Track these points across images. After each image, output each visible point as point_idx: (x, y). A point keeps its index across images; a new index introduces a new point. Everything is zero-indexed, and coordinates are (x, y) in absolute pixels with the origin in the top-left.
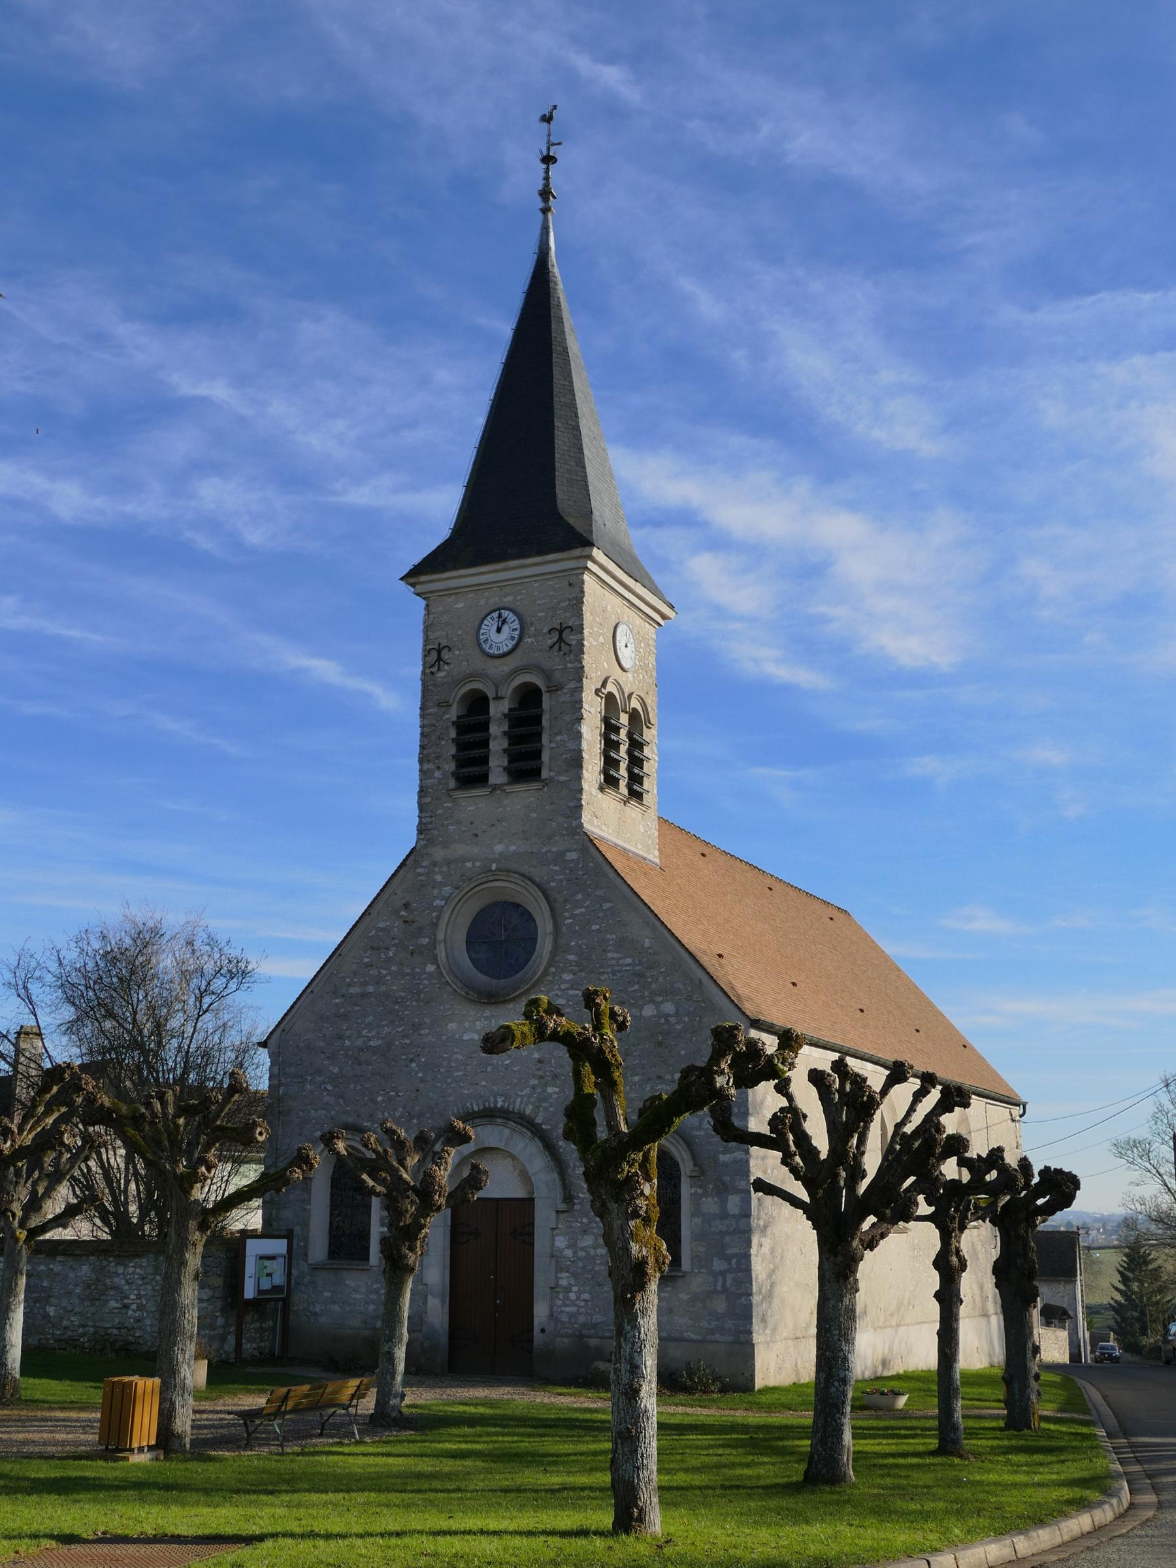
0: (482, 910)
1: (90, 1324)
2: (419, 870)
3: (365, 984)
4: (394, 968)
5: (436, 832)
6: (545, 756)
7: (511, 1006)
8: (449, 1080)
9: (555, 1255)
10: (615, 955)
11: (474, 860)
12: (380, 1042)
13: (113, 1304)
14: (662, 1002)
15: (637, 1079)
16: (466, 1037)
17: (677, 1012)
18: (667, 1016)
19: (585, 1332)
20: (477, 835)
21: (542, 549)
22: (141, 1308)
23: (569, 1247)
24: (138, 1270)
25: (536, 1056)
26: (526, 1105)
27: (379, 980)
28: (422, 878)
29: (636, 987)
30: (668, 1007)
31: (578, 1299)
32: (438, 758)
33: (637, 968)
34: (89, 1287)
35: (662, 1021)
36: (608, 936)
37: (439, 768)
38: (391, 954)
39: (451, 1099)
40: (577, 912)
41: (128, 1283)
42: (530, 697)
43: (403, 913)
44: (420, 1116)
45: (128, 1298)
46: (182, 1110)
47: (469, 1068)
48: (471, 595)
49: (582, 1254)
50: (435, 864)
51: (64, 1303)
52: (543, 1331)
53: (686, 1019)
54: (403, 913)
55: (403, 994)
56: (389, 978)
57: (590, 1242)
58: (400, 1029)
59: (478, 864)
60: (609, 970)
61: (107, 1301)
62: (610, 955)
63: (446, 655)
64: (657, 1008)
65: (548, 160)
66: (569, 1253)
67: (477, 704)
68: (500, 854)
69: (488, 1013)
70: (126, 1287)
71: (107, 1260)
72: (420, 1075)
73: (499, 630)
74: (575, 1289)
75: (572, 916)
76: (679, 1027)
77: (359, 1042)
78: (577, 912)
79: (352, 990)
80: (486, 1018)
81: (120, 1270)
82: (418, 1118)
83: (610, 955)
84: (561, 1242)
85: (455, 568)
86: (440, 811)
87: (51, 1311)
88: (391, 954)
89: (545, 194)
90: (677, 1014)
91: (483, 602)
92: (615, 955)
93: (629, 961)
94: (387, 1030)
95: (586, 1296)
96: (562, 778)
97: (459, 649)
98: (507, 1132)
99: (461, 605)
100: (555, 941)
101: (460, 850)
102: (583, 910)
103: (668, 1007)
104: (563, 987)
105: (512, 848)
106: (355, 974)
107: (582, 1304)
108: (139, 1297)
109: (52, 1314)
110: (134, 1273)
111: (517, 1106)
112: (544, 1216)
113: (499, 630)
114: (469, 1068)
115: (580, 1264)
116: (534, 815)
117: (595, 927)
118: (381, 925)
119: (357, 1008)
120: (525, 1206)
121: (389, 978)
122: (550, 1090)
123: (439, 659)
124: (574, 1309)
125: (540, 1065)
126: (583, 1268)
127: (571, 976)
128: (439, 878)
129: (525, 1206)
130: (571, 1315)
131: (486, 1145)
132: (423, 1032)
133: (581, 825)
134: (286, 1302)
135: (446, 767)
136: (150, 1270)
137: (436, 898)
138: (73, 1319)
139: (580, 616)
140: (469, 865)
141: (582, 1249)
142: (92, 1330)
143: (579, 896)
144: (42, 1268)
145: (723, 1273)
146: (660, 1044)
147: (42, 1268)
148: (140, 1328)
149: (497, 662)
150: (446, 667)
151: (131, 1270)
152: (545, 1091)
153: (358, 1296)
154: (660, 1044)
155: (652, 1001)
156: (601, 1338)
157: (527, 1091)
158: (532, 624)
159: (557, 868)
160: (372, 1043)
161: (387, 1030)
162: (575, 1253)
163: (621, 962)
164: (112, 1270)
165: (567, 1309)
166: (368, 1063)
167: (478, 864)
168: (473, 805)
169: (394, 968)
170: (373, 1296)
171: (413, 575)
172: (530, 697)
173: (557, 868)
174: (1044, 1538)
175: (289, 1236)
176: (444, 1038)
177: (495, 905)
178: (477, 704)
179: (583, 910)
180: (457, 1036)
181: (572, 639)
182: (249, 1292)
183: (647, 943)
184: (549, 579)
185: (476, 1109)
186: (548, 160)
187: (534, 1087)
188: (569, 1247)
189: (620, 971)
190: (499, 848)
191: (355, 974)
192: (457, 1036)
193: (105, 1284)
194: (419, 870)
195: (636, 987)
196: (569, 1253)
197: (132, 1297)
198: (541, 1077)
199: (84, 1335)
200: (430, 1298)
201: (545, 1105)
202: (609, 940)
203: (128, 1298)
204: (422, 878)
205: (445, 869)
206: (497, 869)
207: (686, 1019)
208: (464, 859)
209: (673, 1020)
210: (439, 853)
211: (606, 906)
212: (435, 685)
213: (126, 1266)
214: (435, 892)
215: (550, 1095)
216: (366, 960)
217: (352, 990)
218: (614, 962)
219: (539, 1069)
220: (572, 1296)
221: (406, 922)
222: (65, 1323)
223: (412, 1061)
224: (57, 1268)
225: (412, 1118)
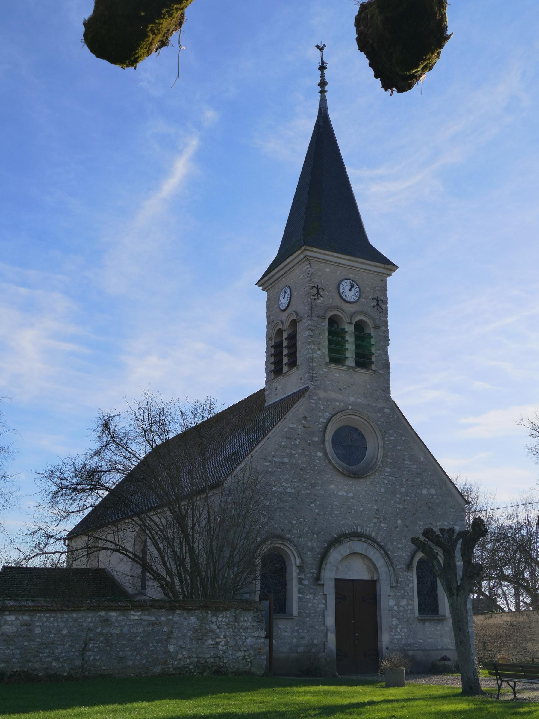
0: (339, 429)
1: (194, 656)
2: (312, 401)
3: (283, 457)
4: (299, 451)
5: (319, 383)
7: (362, 480)
8: (333, 515)
9: (391, 609)
10: (409, 463)
11: (340, 402)
12: (293, 491)
13: (210, 642)
14: (430, 488)
15: (421, 523)
16: (340, 493)
17: (437, 494)
18: (432, 495)
19: (405, 648)
20: (341, 390)
22: (227, 643)
23: (396, 605)
24: (224, 619)
25: (375, 507)
26: (372, 532)
27: (291, 456)
28: (313, 405)
29: (419, 480)
31: (401, 631)
32: (319, 344)
33: (418, 470)
34: (197, 631)
35: (431, 497)
36: (405, 453)
37: (319, 349)
38: (297, 443)
39: (334, 526)
40: (391, 438)
41: (218, 627)
43: (303, 422)
44: (318, 533)
45: (219, 637)
47: (342, 510)
48: (333, 267)
49: (401, 608)
50: (320, 399)
51: (180, 642)
52: (387, 648)
53: (440, 497)
54: (303, 422)
55: (305, 466)
56: (297, 455)
57: (405, 603)
58: (305, 485)
59: (342, 404)
60: (407, 469)
61: (206, 640)
62: (407, 462)
64: (428, 491)
66: (396, 608)
67: (280, 332)
68: (353, 402)
69: (351, 482)
70: (218, 631)
71: (206, 613)
72: (317, 511)
73: (350, 290)
74: (400, 626)
75: (389, 440)
76: (437, 501)
77: (281, 489)
78: (391, 438)
79: (275, 459)
80: (350, 485)
81: (214, 619)
82: (317, 535)
83: (407, 462)
84: (392, 603)
85: (331, 251)
86: (321, 372)
87: (171, 648)
88: (297, 443)
89: (323, 84)
90: (436, 494)
91: (339, 272)
92: (409, 463)
93: (415, 466)
94: (297, 484)
95: (405, 630)
96: (381, 372)
97: (328, 292)
98: (365, 545)
99: (328, 270)
101: (333, 395)
102: (394, 438)
103: (433, 491)
104: (386, 474)
105: (359, 400)
106: (277, 450)
107: (403, 634)
108: (225, 636)
109: (171, 650)
110: (222, 621)
111: (367, 532)
112: (384, 589)
113: (350, 290)
114: (342, 510)
115: (401, 614)
116: (368, 386)
117: (399, 448)
118: (291, 426)
119: (279, 470)
120: (372, 584)
121: (297, 455)
122: (383, 525)
123: (318, 293)
124: (400, 637)
125: (377, 512)
126: (403, 616)
127: (389, 470)
128: (322, 407)
129: (372, 584)
130: (399, 640)
131: (355, 551)
132: (317, 488)
133: (390, 397)
135: (323, 350)
136: (232, 619)
137: (321, 417)
138: (184, 653)
139: (386, 295)
140: (338, 404)
141: (402, 606)
142: (195, 660)
143: (391, 431)
144: (163, 618)
146: (430, 508)
147: (163, 618)
148: (226, 657)
149: (347, 305)
150: (321, 298)
151: (220, 619)
152: (380, 526)
153: (286, 634)
154: (430, 508)
155: (426, 487)
156: (413, 650)
157: (372, 525)
158: (364, 292)
159: (380, 415)
160: (289, 490)
161: (297, 484)
162: (398, 608)
163: (412, 466)
164: (210, 619)
165: (397, 637)
166: (287, 501)
167: (342, 404)
169: (299, 451)
170: (295, 634)
173: (380, 415)
176: (328, 492)
179: (394, 438)
180: (335, 493)
181: (383, 306)
183: (422, 459)
184: (371, 274)
185: (347, 532)
187: (375, 523)
188: (396, 605)
189: (411, 471)
190: (352, 399)
191: (277, 450)
192: (335, 493)
193: (206, 629)
194: (312, 401)
195: (419, 480)
196: (396, 608)
197: (222, 637)
198: (378, 518)
199: (192, 663)
200: (329, 633)
201: (381, 532)
202: (406, 455)
203: (219, 637)
204: (313, 405)
205: (325, 403)
206: (351, 409)
207: (440, 497)
208: (335, 400)
209: (435, 497)
211: (404, 438)
212: (316, 306)
213: (218, 617)
214: (320, 414)
215: (383, 528)
216: (283, 444)
217: (275, 459)
218: (408, 466)
219: (376, 514)
220: (399, 630)
221: (305, 427)
222: (180, 656)
223: (312, 503)
224: (176, 618)
225: (314, 534)
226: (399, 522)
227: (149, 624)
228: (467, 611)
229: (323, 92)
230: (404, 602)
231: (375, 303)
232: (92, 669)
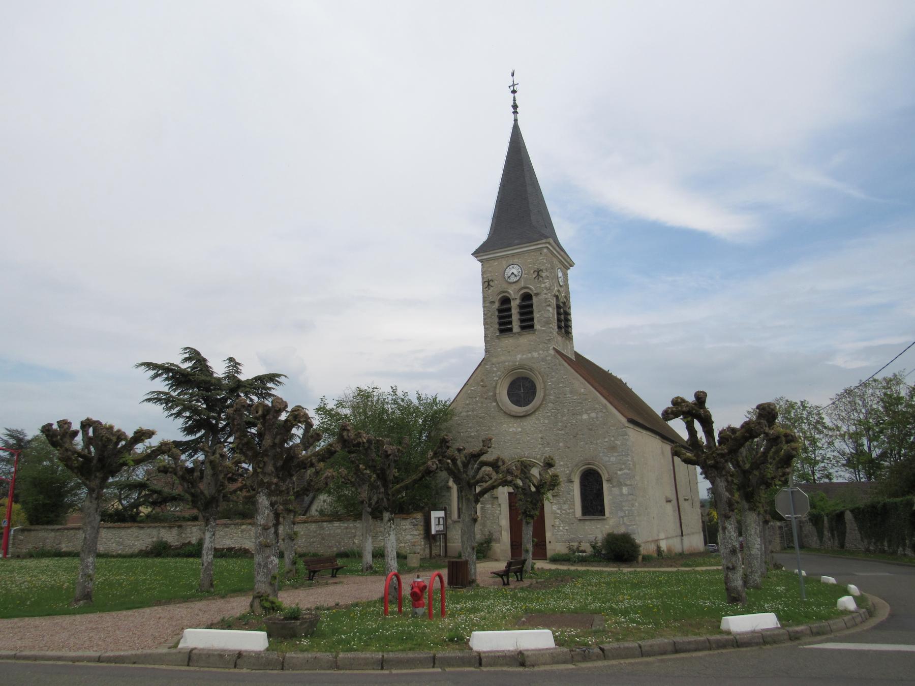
6: (535, 321)
9: (554, 513)
18: (592, 418)
21: (531, 241)
30: (593, 415)
42: (527, 297)
46: (245, 448)
63: (491, 283)
65: (514, 92)
66: (558, 511)
67: (506, 301)
89: (515, 106)
100: (545, 392)
103: (593, 415)
134: (445, 535)
145: (622, 517)
146: (591, 430)
154: (591, 430)
168: (508, 342)
171: (476, 254)
172: (527, 297)
174: (177, 668)
175: (445, 509)
177: (518, 379)
178: (506, 301)
182: (433, 532)
186: (514, 92)
194: (865, 441)
196: (558, 511)
210: (494, 360)
226: (561, 444)
227: (527, 478)
228: (184, 544)
229: (515, 112)
230: (566, 507)
231: (536, 274)
232: (625, 490)
